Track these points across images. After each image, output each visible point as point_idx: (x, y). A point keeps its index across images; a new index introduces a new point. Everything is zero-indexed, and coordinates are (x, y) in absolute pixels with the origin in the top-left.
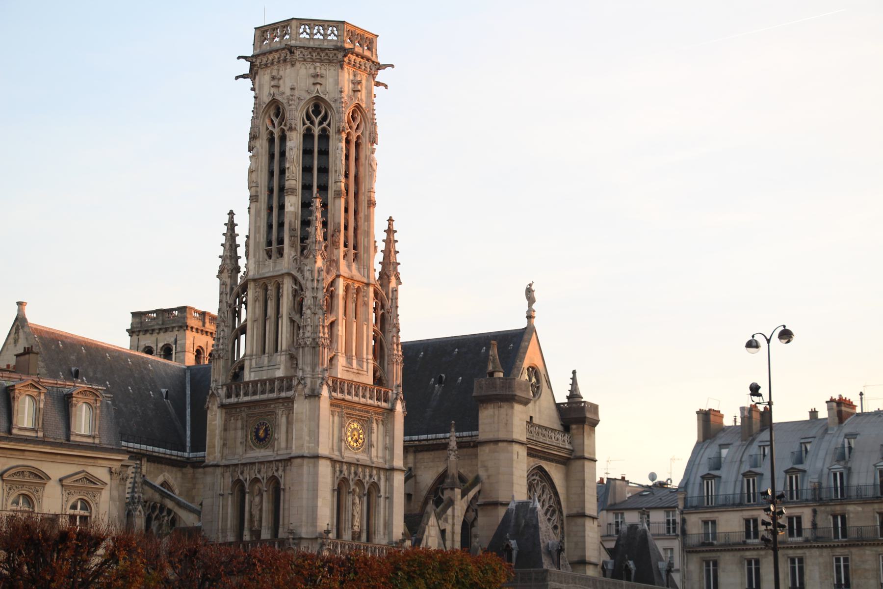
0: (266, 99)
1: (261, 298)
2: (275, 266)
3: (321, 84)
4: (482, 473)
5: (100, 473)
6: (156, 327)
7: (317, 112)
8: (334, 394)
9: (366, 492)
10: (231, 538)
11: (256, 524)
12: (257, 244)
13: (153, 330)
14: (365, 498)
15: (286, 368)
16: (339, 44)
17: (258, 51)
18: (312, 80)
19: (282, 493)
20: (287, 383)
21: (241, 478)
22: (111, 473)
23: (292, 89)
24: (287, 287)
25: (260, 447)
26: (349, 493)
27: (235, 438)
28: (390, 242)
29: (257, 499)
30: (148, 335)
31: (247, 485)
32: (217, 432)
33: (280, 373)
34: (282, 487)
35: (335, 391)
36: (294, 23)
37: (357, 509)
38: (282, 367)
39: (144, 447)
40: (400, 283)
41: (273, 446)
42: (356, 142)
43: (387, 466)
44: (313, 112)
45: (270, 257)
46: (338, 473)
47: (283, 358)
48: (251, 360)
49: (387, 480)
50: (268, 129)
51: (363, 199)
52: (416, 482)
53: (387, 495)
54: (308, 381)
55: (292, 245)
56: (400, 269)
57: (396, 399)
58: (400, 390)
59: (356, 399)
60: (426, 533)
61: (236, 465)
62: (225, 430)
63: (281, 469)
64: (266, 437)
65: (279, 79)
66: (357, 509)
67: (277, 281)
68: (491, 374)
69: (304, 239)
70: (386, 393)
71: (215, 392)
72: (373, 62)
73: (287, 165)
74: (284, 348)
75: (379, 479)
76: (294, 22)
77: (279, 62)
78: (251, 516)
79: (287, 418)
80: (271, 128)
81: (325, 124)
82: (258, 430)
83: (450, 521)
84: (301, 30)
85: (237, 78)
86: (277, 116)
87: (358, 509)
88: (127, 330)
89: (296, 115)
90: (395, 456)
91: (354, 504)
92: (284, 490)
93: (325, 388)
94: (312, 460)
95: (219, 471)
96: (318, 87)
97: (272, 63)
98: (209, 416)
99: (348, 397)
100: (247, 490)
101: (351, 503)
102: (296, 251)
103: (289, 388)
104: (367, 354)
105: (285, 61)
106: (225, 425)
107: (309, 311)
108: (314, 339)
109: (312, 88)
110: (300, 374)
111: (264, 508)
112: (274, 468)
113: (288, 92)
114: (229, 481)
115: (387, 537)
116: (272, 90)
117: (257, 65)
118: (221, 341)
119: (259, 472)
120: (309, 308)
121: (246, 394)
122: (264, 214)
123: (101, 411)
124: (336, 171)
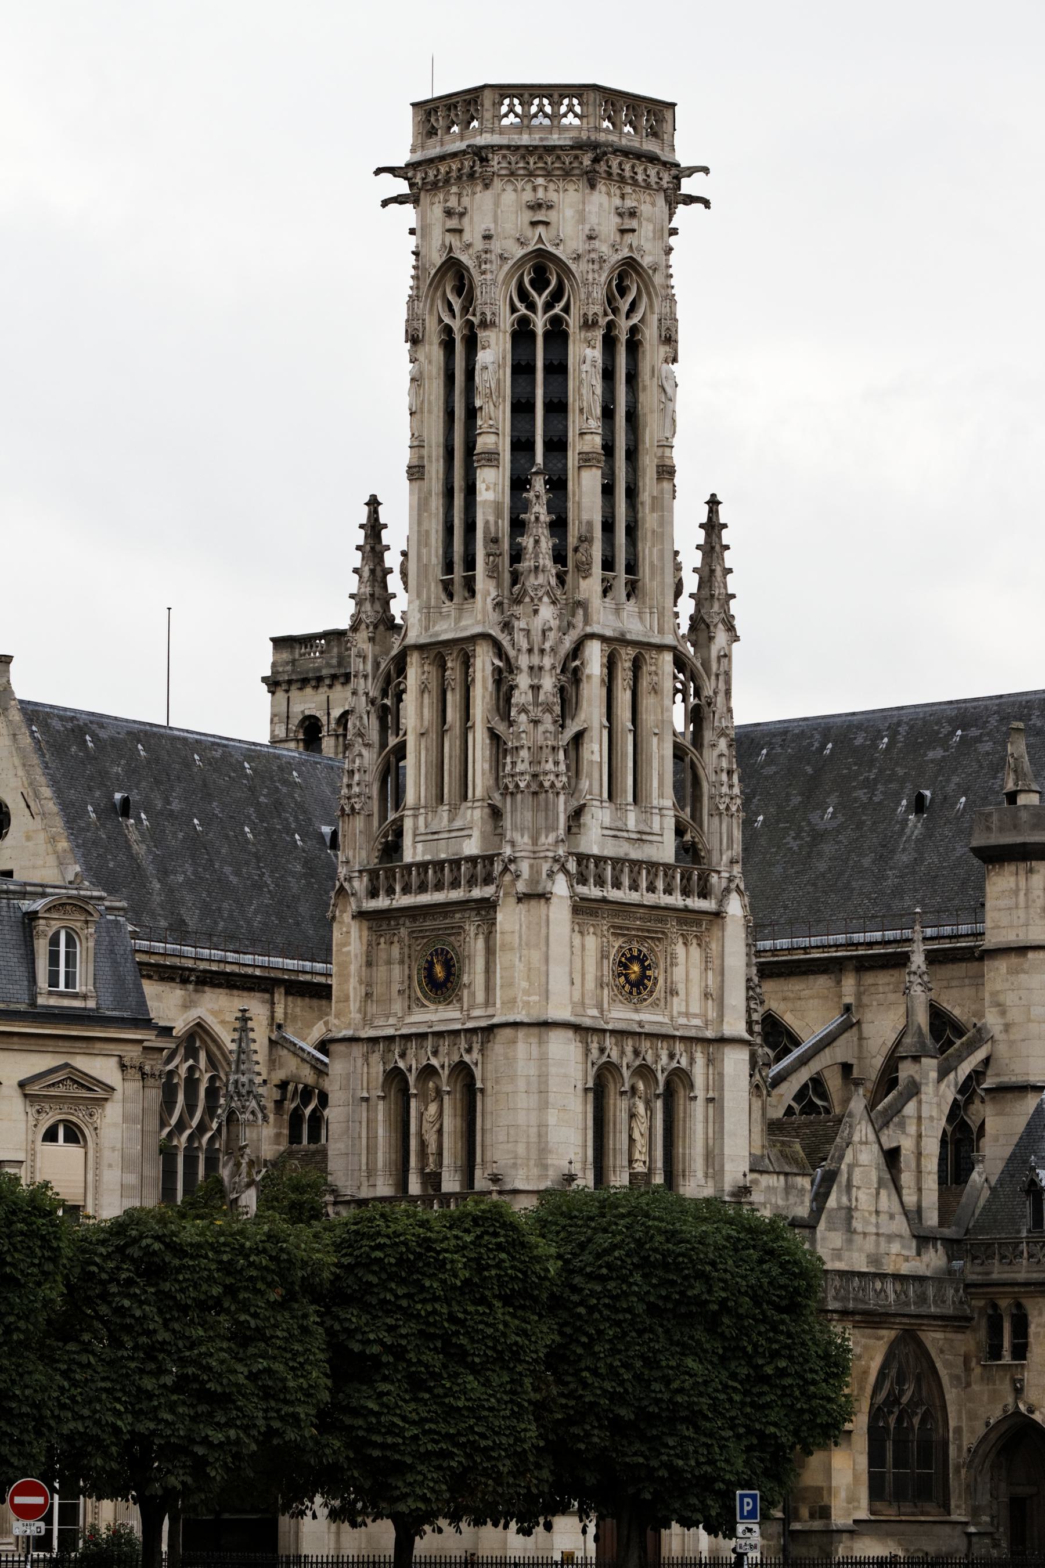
0: (437, 259)
1: (434, 685)
2: (458, 619)
3: (547, 224)
4: (992, 1020)
5: (102, 1068)
6: (325, 672)
7: (540, 282)
8: (582, 890)
9: (661, 1090)
10: (384, 1188)
11: (431, 1159)
12: (424, 569)
13: (319, 679)
14: (659, 1104)
15: (484, 836)
16: (584, 136)
17: (418, 157)
18: (528, 216)
19: (479, 1096)
20: (484, 867)
21: (401, 1065)
22: (123, 1067)
23: (487, 237)
24: (484, 662)
25: (436, 1001)
26: (622, 1093)
27: (389, 983)
28: (713, 546)
29: (433, 1108)
30: (309, 691)
31: (412, 1079)
32: (353, 968)
33: (471, 847)
34: (479, 1085)
35: (583, 880)
36: (488, 98)
37: (637, 1130)
38: (476, 833)
39: (278, 961)
40: (736, 639)
41: (460, 1000)
42: (628, 341)
43: (709, 1034)
44: (532, 282)
45: (451, 596)
46: (595, 1052)
47: (477, 813)
48: (415, 816)
49: (710, 1061)
50: (441, 321)
51: (648, 463)
52: (861, 1038)
53: (711, 1095)
54: (525, 867)
55: (493, 573)
56: (734, 606)
57: (727, 891)
58: (737, 869)
59: (634, 897)
60: (848, 1158)
61: (390, 1039)
62: (369, 964)
63: (476, 1047)
64: (447, 979)
65: (462, 215)
66: (637, 1130)
67: (463, 648)
68: (1012, 797)
69: (516, 556)
70: (704, 878)
71: (346, 885)
72: (665, 164)
73: (478, 403)
74: (479, 793)
75: (692, 1061)
76: (487, 92)
77: (459, 178)
78: (423, 1145)
79: (487, 941)
80: (447, 320)
81: (557, 310)
82: (431, 966)
83: (912, 1129)
84: (504, 109)
85: (385, 203)
86: (459, 291)
87: (640, 1127)
88: (264, 680)
89: (496, 296)
90: (727, 1012)
91: (632, 1116)
92: (482, 1090)
93: (561, 880)
94: (535, 1031)
95: (358, 1050)
96: (541, 229)
97: (447, 181)
98: (336, 935)
99: (614, 894)
100: (413, 1091)
101: (625, 1116)
102: (499, 585)
103: (488, 880)
104: (661, 796)
105: (472, 176)
106: (368, 954)
107: (523, 717)
108: (535, 776)
109: (529, 232)
110: (508, 851)
111: (446, 1129)
112: (463, 1045)
113: (479, 245)
114: (378, 1069)
115: (711, 1183)
116: (450, 238)
117: (423, 180)
118: (357, 777)
119: (435, 1053)
120: (524, 710)
121: (406, 890)
122: (436, 504)
123: (97, 943)
124: (581, 410)
